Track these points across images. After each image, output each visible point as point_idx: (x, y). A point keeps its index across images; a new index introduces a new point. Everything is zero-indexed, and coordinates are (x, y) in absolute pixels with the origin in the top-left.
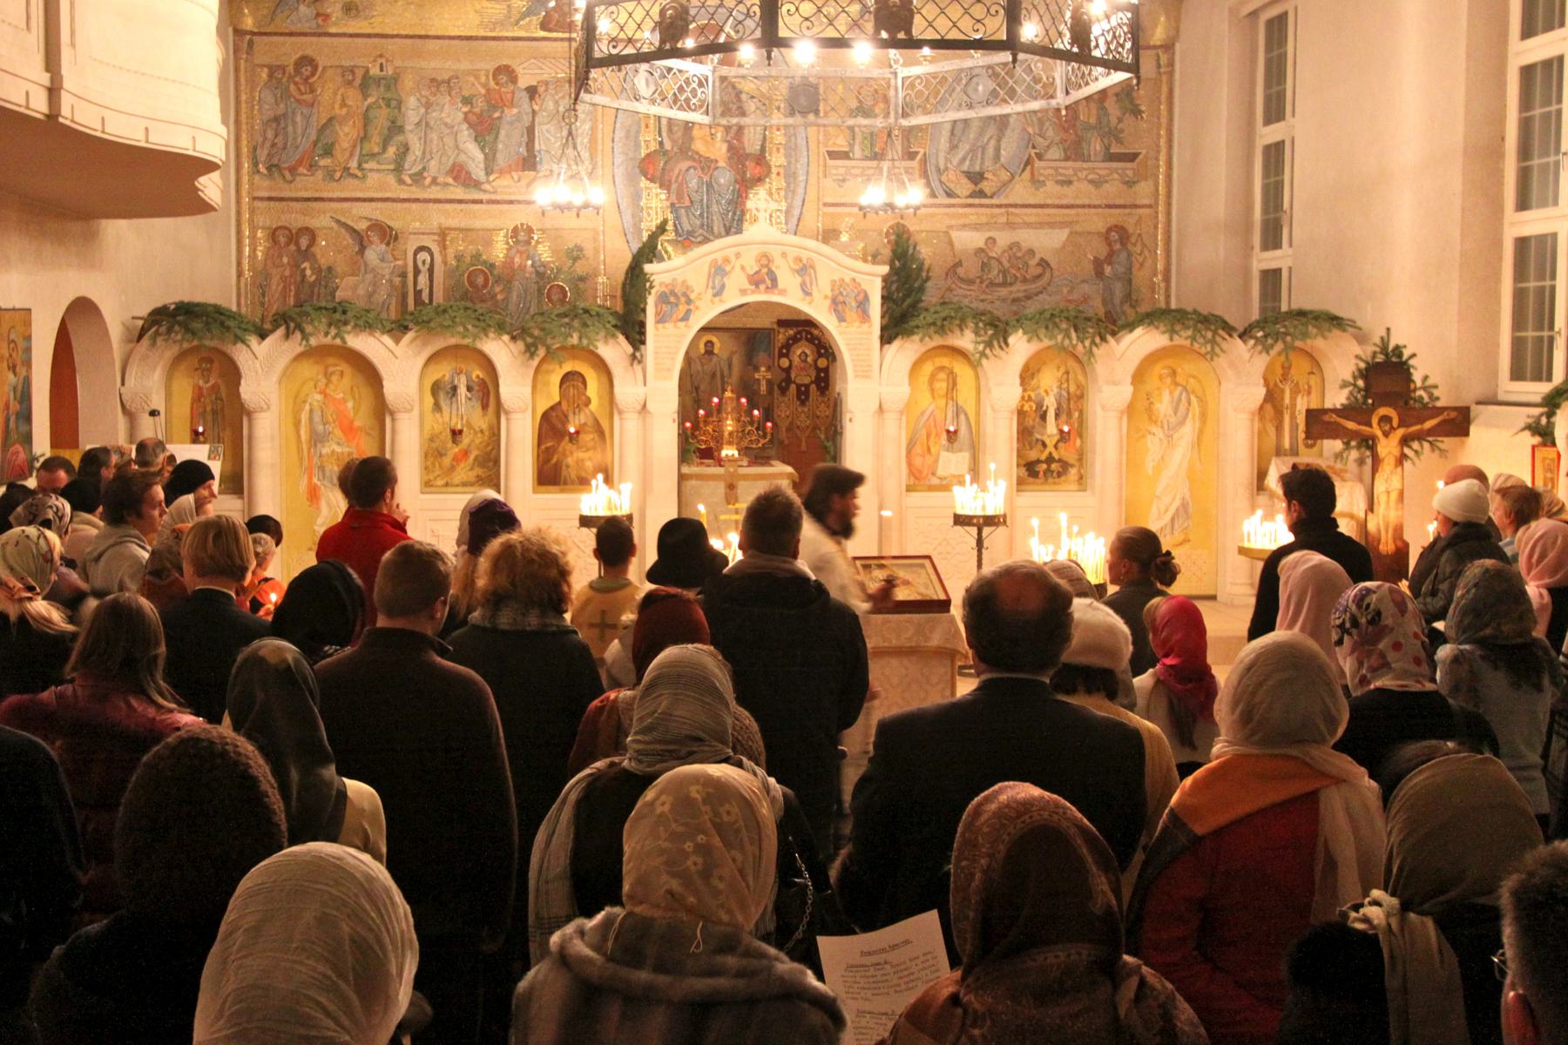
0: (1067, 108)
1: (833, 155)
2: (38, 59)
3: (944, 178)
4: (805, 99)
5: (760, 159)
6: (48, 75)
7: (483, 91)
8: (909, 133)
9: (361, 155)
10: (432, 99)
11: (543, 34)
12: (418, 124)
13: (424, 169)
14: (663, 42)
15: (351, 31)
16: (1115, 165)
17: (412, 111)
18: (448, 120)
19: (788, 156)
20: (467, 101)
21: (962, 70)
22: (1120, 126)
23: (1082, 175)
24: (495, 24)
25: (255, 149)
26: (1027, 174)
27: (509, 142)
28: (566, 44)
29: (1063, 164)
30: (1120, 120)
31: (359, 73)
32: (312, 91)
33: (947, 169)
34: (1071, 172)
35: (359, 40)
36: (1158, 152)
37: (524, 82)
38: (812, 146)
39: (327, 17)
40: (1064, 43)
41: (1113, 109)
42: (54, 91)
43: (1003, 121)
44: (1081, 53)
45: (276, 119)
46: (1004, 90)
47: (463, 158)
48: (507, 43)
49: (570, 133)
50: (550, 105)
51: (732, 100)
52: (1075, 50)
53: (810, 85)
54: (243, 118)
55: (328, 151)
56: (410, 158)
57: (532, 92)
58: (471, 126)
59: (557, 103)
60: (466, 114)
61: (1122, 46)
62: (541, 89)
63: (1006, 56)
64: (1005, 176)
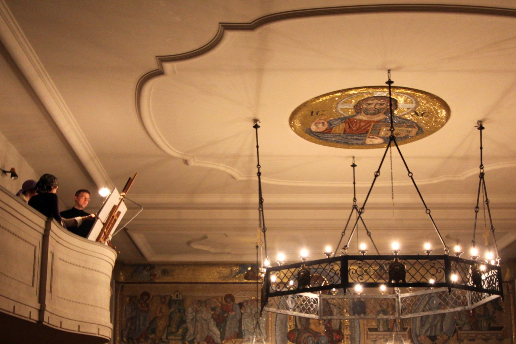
0: (472, 310)
1: (371, 330)
2: (36, 298)
3: (419, 339)
4: (360, 307)
5: (339, 332)
6: (39, 305)
7: (220, 305)
8: (402, 320)
9: (168, 333)
10: (198, 309)
11: (245, 281)
12: (192, 319)
13: (194, 338)
14: (299, 286)
15: (165, 281)
16: (492, 332)
17: (190, 313)
18: (205, 318)
19: (351, 330)
20: (213, 309)
21: (426, 295)
22: (494, 315)
23: (479, 336)
24: (225, 277)
25: (122, 331)
26: (455, 336)
27: (231, 327)
28: (256, 285)
29: (471, 332)
30: (494, 313)
31: (168, 298)
32: (148, 306)
33: (420, 335)
34: (474, 335)
35: (168, 285)
36: (512, 326)
37: (237, 301)
38: (362, 326)
39: (155, 275)
40: (470, 283)
41: (491, 309)
42: (41, 311)
43: (443, 315)
44: (477, 287)
45: (132, 318)
46: (444, 303)
47: (211, 333)
48: (230, 285)
49: (258, 323)
50: (249, 310)
51: (326, 309)
52: (475, 286)
53: (361, 302)
54: (118, 318)
55: (154, 332)
56: (188, 334)
57: (241, 305)
58: (215, 320)
59: (251, 310)
60: (213, 315)
61: (495, 284)
62: (245, 304)
63: (446, 289)
64: (445, 337)
